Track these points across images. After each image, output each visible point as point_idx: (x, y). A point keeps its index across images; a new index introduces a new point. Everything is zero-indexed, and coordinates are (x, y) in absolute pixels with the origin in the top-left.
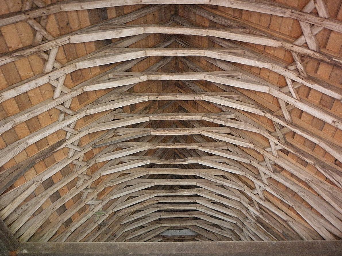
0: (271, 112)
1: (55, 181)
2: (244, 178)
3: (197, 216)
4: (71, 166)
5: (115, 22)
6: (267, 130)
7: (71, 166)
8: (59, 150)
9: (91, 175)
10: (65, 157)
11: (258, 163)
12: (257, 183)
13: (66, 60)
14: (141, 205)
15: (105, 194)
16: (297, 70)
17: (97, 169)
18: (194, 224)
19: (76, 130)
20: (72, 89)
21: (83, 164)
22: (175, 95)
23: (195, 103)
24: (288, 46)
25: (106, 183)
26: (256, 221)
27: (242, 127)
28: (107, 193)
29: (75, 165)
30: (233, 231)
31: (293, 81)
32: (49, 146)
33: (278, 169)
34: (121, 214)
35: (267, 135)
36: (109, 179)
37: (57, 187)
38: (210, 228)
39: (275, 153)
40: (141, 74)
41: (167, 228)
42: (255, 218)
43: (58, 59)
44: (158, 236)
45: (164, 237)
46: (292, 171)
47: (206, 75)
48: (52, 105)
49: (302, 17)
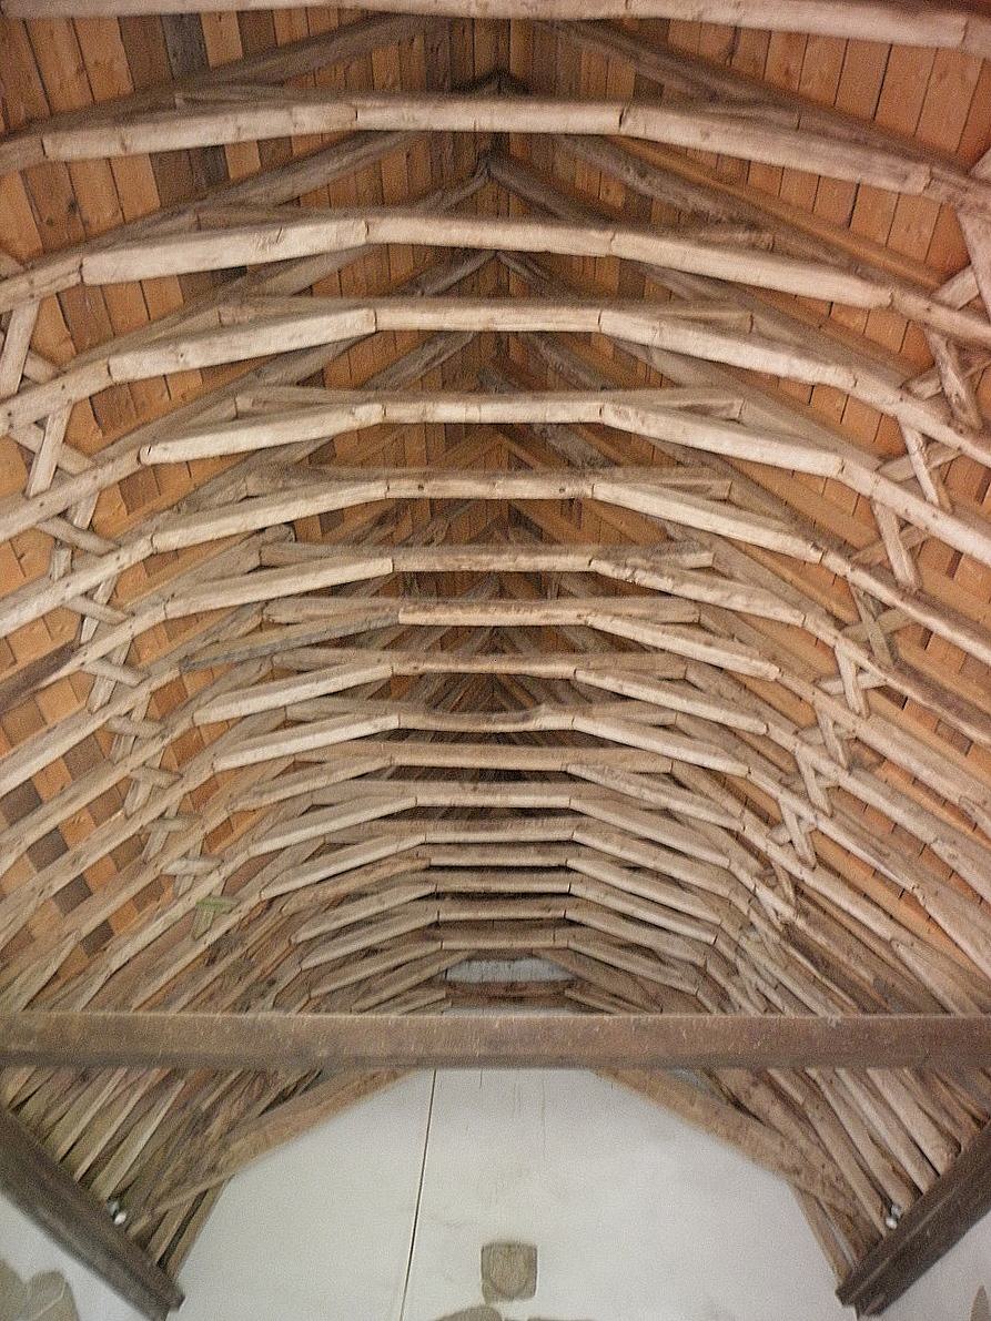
0: (845, 549)
1: (44, 795)
2: (741, 785)
3: (571, 915)
4: (101, 737)
5: (256, 193)
6: (829, 614)
7: (101, 737)
8: (54, 683)
9: (176, 769)
10: (78, 707)
11: (796, 733)
12: (789, 804)
13: (70, 346)
14: (367, 873)
15: (233, 837)
16: (941, 397)
17: (200, 746)
18: (561, 943)
19: (115, 608)
20: (95, 458)
21: (148, 729)
22: (489, 477)
23: (572, 507)
24: (914, 304)
25: (233, 799)
26: (783, 937)
27: (738, 603)
28: (238, 832)
29: (115, 736)
30: (702, 971)
31: (929, 440)
32: (19, 666)
33: (868, 756)
34: (291, 907)
35: (827, 633)
36: (245, 783)
37: (53, 816)
38: (621, 957)
39: (856, 700)
40: (359, 395)
41: (461, 956)
42: (781, 929)
43: (39, 341)
44: (429, 983)
45: (452, 985)
46: (915, 766)
47: (607, 405)
48: (23, 518)
49: (970, 198)
